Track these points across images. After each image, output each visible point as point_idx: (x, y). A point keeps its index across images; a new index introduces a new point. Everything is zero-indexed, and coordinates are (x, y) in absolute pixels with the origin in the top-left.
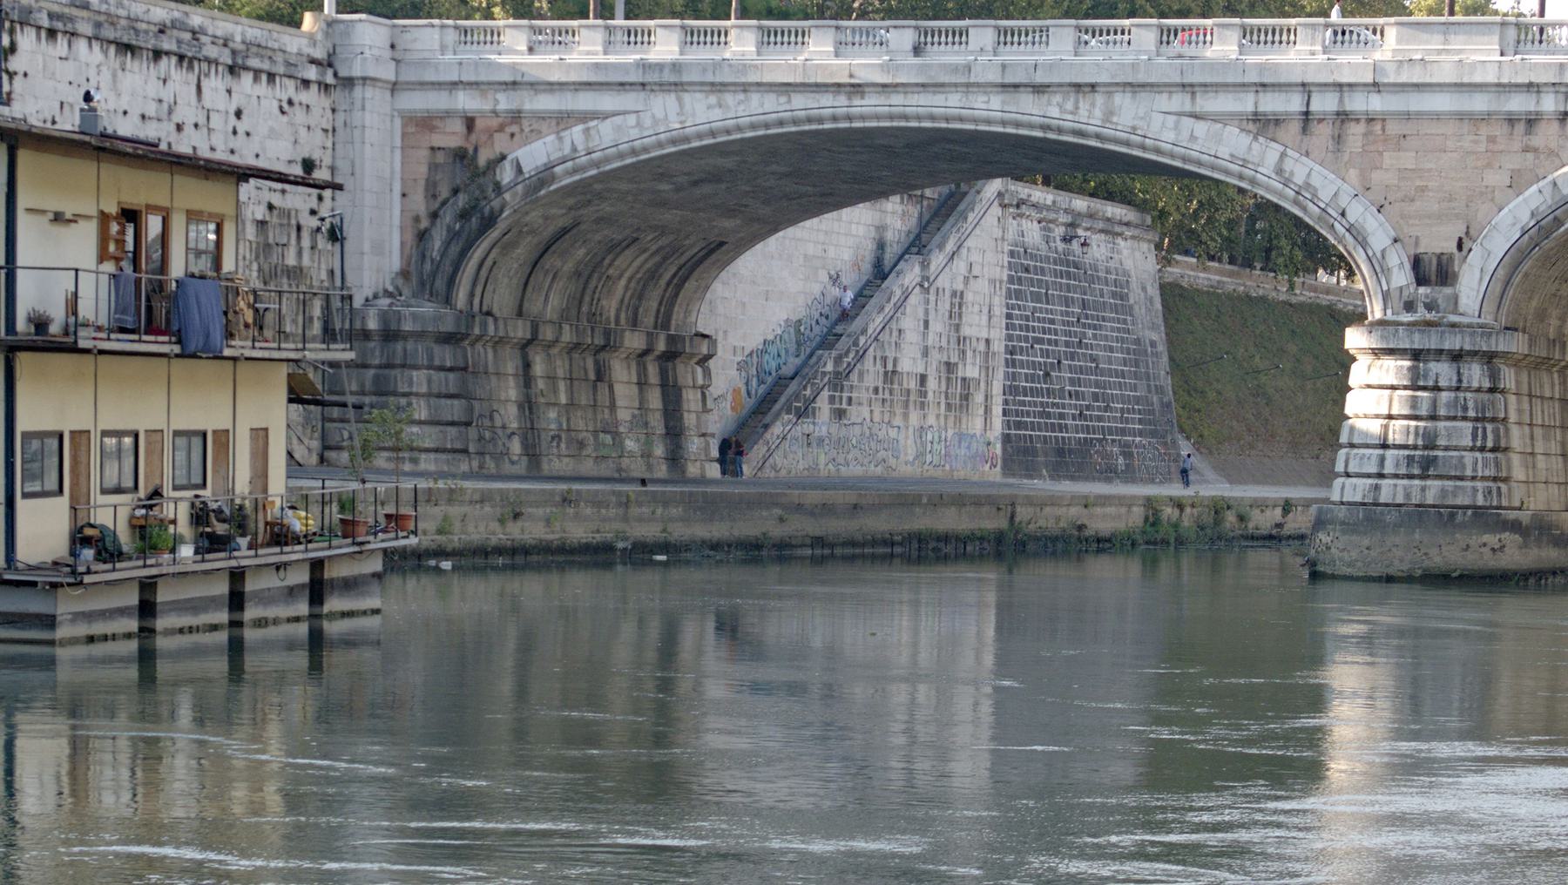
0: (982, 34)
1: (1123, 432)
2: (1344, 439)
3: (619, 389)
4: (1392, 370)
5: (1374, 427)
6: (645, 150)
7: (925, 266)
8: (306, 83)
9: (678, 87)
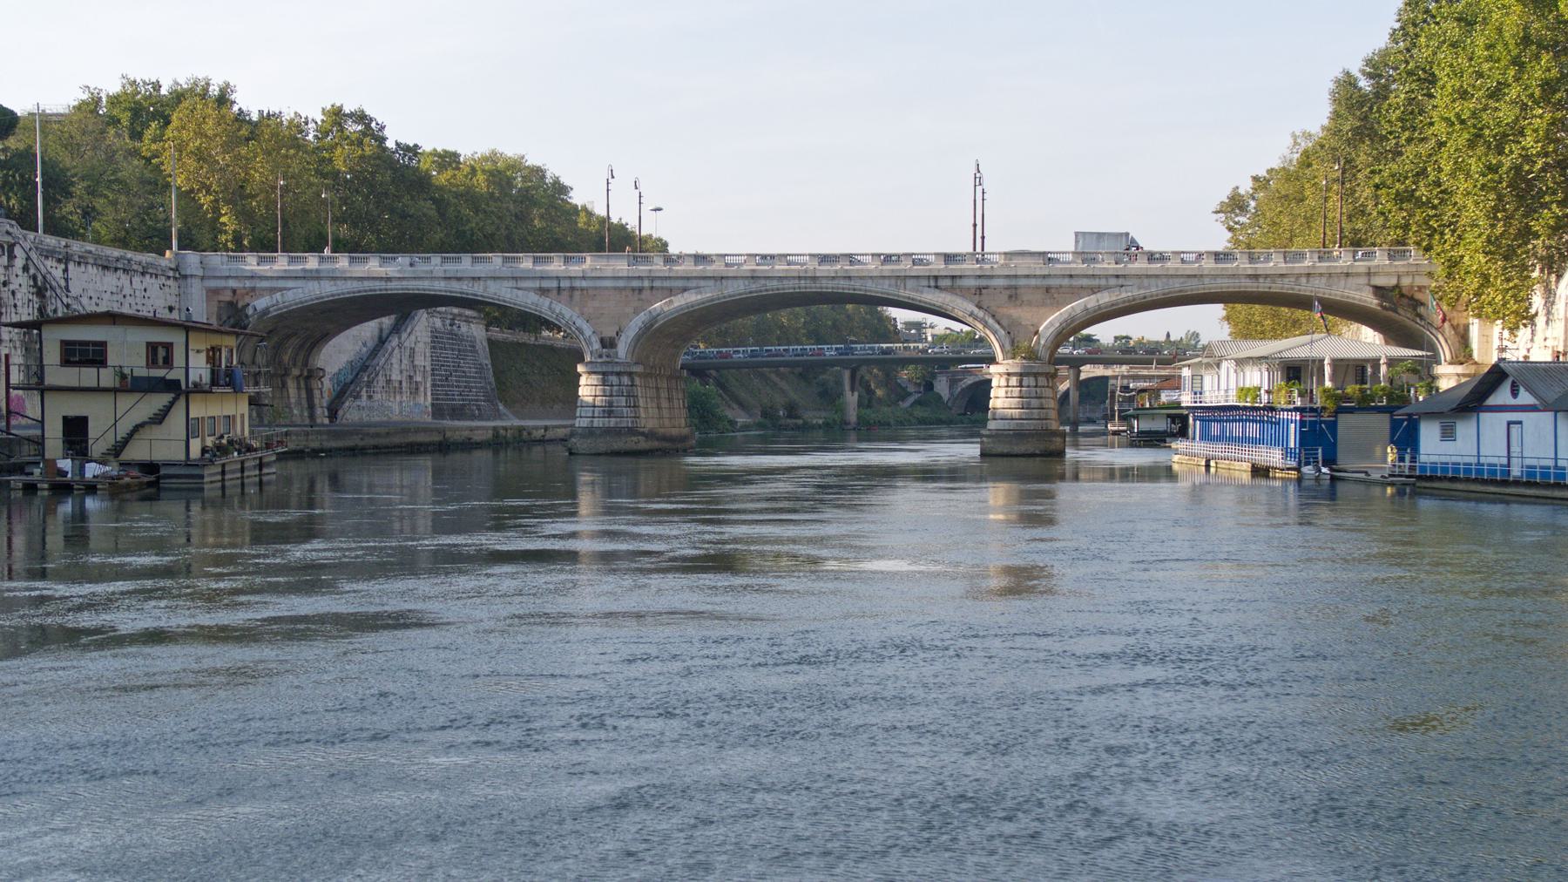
0: (436, 259)
1: (477, 400)
2: (579, 404)
3: (290, 390)
4: (594, 379)
5: (590, 399)
6: (306, 301)
7: (400, 338)
8: (169, 278)
9: (318, 278)
